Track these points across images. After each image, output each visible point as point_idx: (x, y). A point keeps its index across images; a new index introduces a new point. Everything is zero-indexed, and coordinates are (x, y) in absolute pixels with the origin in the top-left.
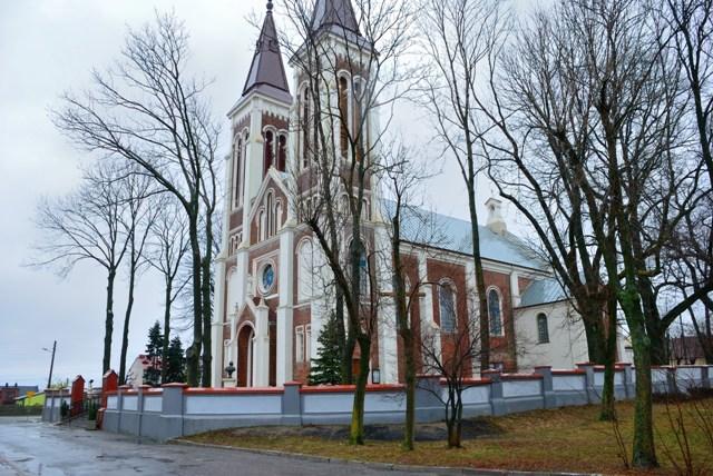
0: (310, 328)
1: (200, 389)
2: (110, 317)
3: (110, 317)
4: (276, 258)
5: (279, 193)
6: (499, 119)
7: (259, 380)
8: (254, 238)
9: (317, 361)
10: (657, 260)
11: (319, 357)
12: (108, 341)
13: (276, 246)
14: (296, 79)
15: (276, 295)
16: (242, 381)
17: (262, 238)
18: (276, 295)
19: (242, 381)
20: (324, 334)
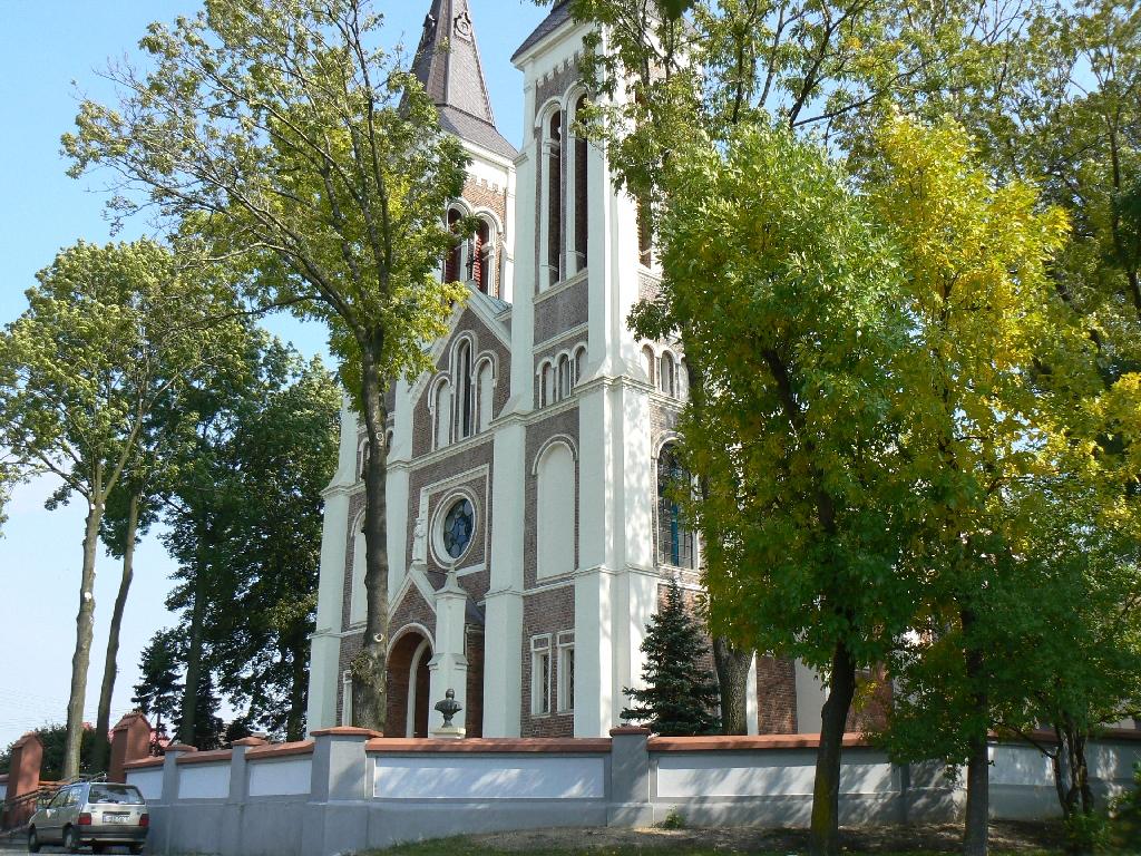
0: (570, 638)
1: (409, 741)
2: (86, 608)
3: (86, 608)
4: (482, 487)
5: (489, 340)
6: (831, 25)
7: (500, 722)
8: (422, 441)
9: (641, 695)
10: (745, 497)
11: (644, 686)
12: (80, 660)
13: (485, 453)
14: (532, 93)
15: (481, 567)
16: (475, 726)
17: (443, 439)
18: (481, 567)
19: (475, 726)
20: (648, 642)
